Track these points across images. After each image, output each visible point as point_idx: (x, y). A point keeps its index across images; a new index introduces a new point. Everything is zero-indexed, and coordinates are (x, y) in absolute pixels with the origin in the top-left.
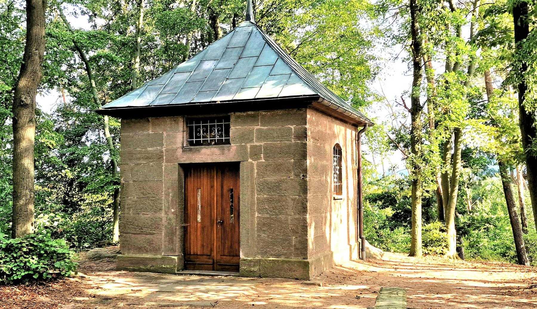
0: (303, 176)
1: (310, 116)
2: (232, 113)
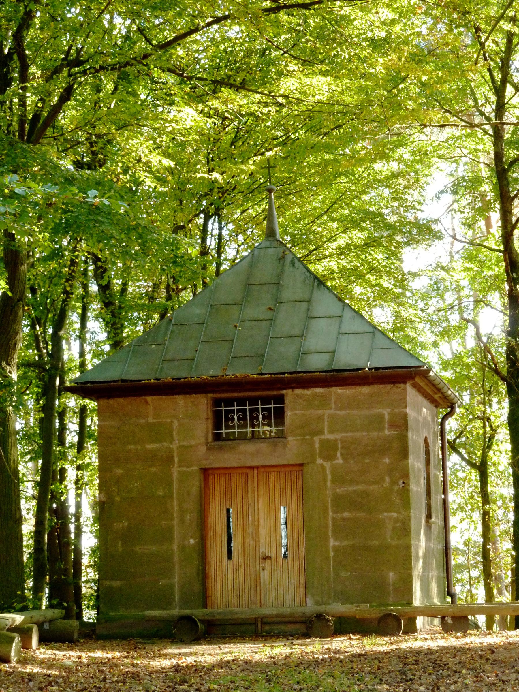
0: (403, 483)
1: (411, 393)
2: (289, 391)
